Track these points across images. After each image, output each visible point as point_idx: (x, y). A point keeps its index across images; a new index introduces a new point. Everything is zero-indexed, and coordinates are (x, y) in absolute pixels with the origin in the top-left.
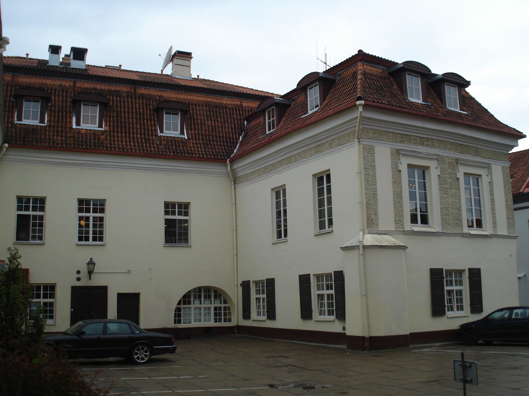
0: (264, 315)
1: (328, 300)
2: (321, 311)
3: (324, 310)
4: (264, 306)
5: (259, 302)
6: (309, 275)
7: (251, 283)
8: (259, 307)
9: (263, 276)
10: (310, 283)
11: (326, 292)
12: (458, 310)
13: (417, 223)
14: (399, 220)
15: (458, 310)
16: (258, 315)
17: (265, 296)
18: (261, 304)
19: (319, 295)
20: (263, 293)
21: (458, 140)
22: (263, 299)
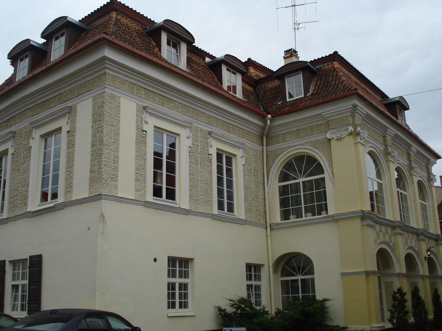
0: (22, 309)
1: (179, 290)
2: (14, 305)
3: (18, 304)
4: (23, 296)
5: (17, 291)
6: (4, 261)
7: (7, 265)
8: (15, 299)
9: (25, 253)
10: (4, 272)
11: (20, 282)
12: (180, 307)
13: (161, 196)
14: (139, 189)
15: (180, 307)
16: (13, 309)
17: (26, 282)
18: (20, 293)
19: (13, 286)
20: (23, 279)
21: (36, 101)
22: (23, 286)
